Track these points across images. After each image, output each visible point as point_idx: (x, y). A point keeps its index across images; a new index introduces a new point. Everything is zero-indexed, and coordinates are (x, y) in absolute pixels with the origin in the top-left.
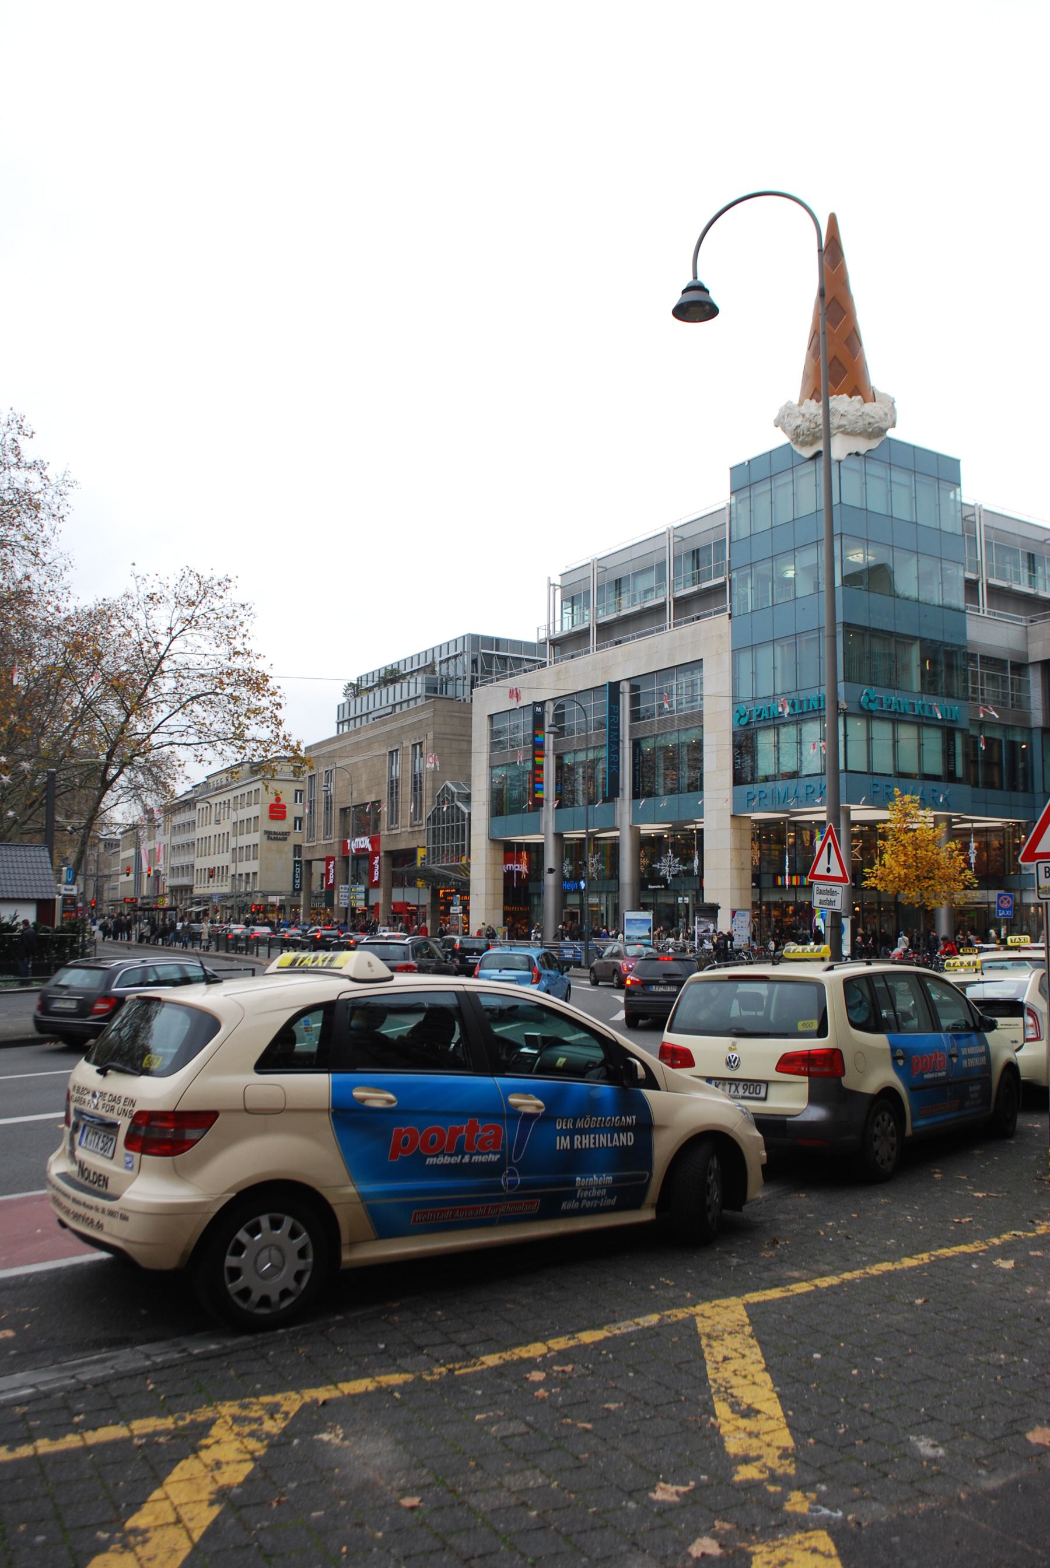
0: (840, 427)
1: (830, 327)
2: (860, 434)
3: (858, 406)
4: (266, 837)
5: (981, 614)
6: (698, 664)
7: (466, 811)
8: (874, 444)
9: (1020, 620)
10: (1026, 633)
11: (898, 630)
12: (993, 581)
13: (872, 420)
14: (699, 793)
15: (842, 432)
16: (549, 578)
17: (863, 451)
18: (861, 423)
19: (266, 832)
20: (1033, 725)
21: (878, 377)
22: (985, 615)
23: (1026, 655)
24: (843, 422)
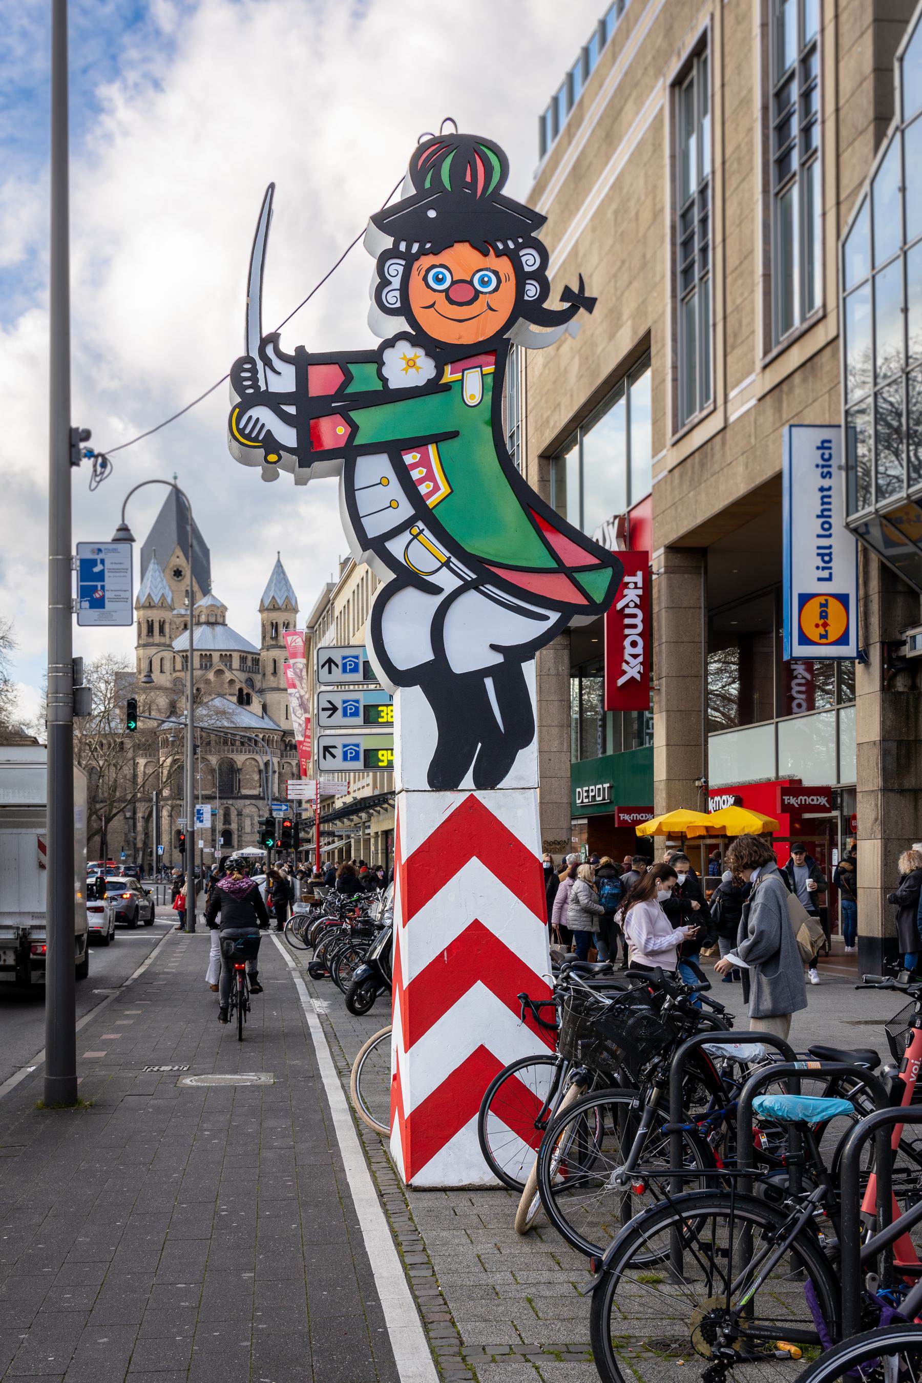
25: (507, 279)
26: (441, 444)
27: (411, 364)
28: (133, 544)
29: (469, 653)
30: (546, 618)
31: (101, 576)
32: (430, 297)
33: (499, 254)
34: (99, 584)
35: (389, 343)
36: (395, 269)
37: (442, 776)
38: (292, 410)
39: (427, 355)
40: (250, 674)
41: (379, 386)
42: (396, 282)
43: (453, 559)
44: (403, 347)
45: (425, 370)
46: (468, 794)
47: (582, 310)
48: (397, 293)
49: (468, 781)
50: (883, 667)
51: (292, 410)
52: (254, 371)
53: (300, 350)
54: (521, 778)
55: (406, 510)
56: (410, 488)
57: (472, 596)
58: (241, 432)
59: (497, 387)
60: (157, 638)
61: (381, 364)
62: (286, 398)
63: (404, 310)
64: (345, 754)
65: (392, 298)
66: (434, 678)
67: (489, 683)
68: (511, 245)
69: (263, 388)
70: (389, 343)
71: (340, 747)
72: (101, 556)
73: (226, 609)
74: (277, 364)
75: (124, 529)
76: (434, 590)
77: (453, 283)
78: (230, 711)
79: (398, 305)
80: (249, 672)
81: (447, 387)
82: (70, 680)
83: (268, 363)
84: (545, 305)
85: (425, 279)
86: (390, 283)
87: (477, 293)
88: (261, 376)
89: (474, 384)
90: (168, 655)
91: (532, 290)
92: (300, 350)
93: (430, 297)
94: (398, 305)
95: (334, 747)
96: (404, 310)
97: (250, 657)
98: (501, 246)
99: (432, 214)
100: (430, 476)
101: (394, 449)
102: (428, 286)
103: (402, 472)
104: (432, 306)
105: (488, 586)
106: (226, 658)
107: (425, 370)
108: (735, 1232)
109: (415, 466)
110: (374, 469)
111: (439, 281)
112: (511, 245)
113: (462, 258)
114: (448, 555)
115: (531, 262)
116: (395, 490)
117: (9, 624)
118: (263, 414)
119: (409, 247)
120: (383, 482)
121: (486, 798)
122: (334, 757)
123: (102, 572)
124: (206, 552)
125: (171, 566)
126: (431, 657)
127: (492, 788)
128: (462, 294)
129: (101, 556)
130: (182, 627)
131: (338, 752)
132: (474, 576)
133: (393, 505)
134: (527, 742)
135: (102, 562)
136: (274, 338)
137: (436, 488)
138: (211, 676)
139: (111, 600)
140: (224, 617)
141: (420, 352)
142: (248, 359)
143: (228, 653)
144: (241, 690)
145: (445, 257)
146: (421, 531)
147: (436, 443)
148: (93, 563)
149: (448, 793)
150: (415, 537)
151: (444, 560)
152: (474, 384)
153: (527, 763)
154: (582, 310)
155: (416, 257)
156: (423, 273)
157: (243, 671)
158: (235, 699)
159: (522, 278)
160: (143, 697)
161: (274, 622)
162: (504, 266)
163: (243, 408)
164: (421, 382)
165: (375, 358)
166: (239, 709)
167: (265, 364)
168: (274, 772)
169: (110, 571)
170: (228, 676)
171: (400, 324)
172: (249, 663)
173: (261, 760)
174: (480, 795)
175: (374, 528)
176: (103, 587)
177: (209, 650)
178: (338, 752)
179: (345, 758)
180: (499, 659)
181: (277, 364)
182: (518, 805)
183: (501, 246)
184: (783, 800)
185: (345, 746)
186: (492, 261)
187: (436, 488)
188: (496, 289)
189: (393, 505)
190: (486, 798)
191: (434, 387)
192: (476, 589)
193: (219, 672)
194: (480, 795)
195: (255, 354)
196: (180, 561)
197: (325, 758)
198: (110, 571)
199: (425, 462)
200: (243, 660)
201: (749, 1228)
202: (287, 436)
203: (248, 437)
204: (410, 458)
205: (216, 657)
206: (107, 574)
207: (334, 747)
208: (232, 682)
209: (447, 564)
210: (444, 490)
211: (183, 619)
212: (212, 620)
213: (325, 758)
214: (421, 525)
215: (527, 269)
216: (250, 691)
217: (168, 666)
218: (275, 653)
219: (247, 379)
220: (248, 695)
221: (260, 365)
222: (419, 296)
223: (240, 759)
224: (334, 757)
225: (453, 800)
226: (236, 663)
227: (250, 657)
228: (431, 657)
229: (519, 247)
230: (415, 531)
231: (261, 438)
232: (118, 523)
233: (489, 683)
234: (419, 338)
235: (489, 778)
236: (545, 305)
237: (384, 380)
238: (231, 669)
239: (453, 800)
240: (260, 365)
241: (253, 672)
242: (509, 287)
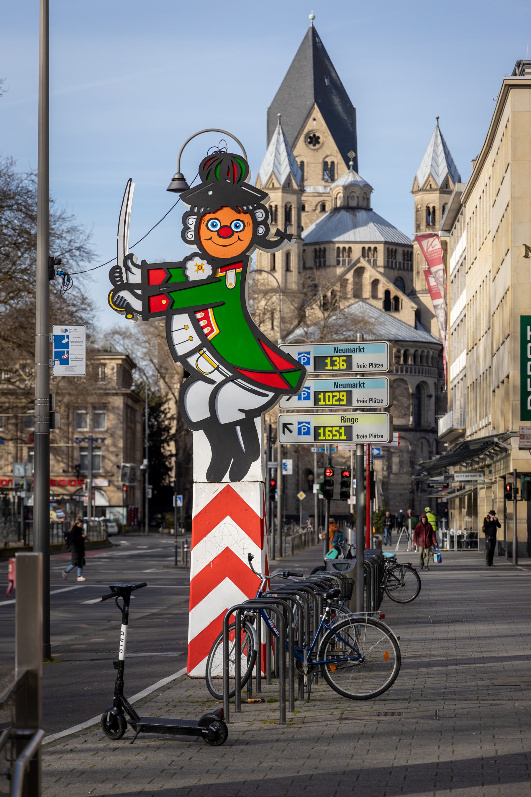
25: (249, 225)
26: (215, 309)
27: (200, 268)
29: (227, 415)
30: (267, 395)
31: (67, 346)
32: (209, 235)
33: (245, 213)
34: (66, 350)
35: (189, 258)
36: (192, 221)
37: (214, 476)
38: (139, 292)
39: (208, 263)
40: (401, 272)
41: (183, 279)
42: (192, 227)
43: (220, 366)
44: (197, 260)
45: (207, 271)
46: (226, 484)
47: (286, 240)
48: (193, 233)
49: (226, 478)
51: (139, 292)
52: (121, 273)
53: (144, 262)
54: (253, 476)
55: (197, 342)
56: (199, 330)
57: (230, 385)
58: (114, 303)
59: (242, 279)
61: (185, 268)
62: (137, 286)
63: (198, 241)
64: (300, 429)
65: (190, 235)
66: (211, 425)
67: (238, 428)
68: (251, 208)
69: (125, 281)
70: (189, 258)
71: (295, 424)
72: (67, 333)
73: (371, 189)
74: (134, 269)
76: (211, 382)
77: (221, 227)
78: (373, 320)
79: (193, 239)
80: (400, 269)
81: (219, 280)
82: (48, 408)
83: (128, 269)
84: (267, 238)
85: (207, 225)
86: (189, 228)
87: (233, 232)
88: (124, 275)
89: (231, 278)
91: (261, 230)
92: (144, 262)
93: (209, 235)
94: (193, 239)
95: (291, 424)
96: (198, 241)
97: (400, 250)
98: (245, 208)
99: (211, 193)
100: (209, 325)
101: (192, 312)
102: (208, 229)
103: (195, 322)
104: (210, 239)
105: (239, 380)
107: (207, 271)
108: (287, 680)
109: (201, 319)
110: (181, 321)
111: (214, 226)
112: (251, 208)
113: (226, 216)
114: (218, 364)
115: (260, 216)
116: (192, 332)
117: (87, 232)
118: (125, 294)
119: (199, 210)
120: (186, 327)
121: (235, 486)
122: (291, 432)
123: (68, 342)
124: (351, 111)
125: (306, 131)
126: (209, 415)
127: (239, 481)
128: (225, 232)
129: (67, 333)
130: (319, 208)
131: (294, 428)
132: (231, 375)
133: (190, 339)
134: (256, 459)
135: (68, 337)
136: (130, 256)
137: (212, 330)
139: (73, 360)
140: (368, 199)
141: (205, 262)
142: (118, 267)
143: (372, 246)
144: (387, 293)
145: (218, 214)
146: (205, 352)
147: (213, 308)
148: (62, 337)
149: (216, 484)
150: (201, 355)
151: (216, 366)
152: (231, 278)
153: (256, 470)
154: (286, 240)
155: (205, 214)
156: (206, 222)
157: (392, 268)
158: (380, 304)
159: (256, 224)
160: (263, 303)
161: (431, 206)
162: (247, 218)
163: (115, 291)
164: (205, 277)
165: (182, 266)
166: (385, 317)
167: (126, 270)
168: (430, 396)
169: (73, 342)
171: (194, 248)
172: (400, 258)
174: (233, 485)
175: (181, 350)
176: (68, 352)
177: (348, 242)
178: (294, 428)
179: (300, 433)
180: (243, 416)
181: (134, 269)
182: (250, 491)
183: (245, 208)
185: (299, 423)
186: (242, 216)
187: (212, 330)
188: (243, 230)
189: (190, 339)
190: (235, 486)
191: (212, 280)
192: (232, 381)
194: (233, 485)
195: (121, 264)
196: (317, 123)
197: (284, 432)
198: (73, 342)
199: (207, 317)
202: (137, 305)
203: (117, 306)
204: (199, 315)
206: (70, 344)
207: (291, 424)
209: (217, 368)
210: (216, 331)
211: (321, 199)
212: (353, 203)
213: (284, 432)
214: (205, 349)
215: (259, 220)
216: (400, 294)
219: (117, 277)
220: (396, 299)
221: (124, 270)
222: (204, 234)
224: (291, 432)
225: (219, 487)
227: (400, 250)
228: (209, 415)
229: (255, 209)
230: (202, 352)
231: (124, 305)
232: (174, 174)
233: (238, 428)
234: (204, 255)
235: (237, 477)
236: (267, 238)
237: (187, 277)
238: (375, 265)
239: (219, 487)
240: (124, 270)
241: (404, 269)
242: (249, 230)
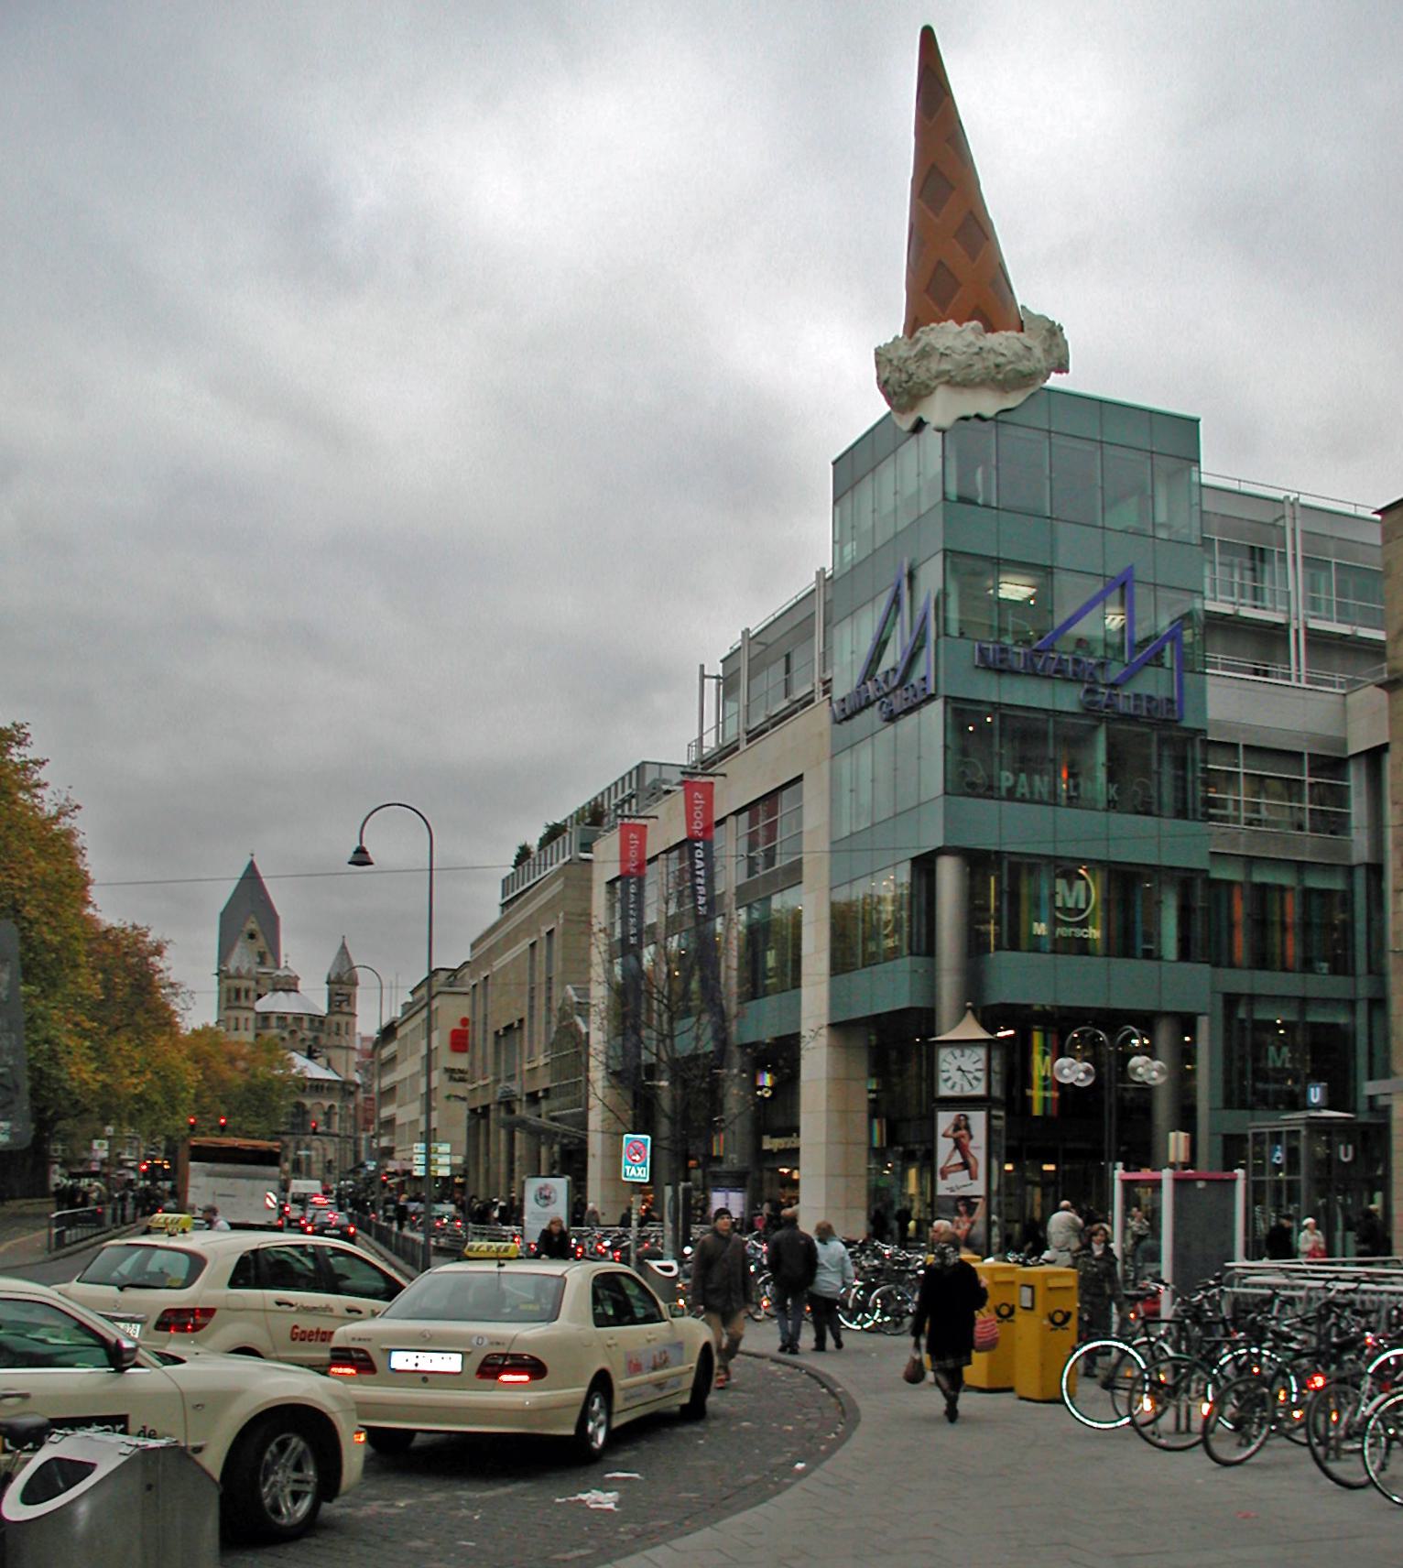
0: (939, 375)
1: (931, 215)
2: (982, 384)
3: (971, 337)
4: (446, 1077)
5: (1293, 683)
6: (799, 778)
7: (584, 1030)
8: (1013, 400)
9: (1332, 684)
10: (1344, 704)
11: (1058, 708)
12: (1313, 624)
13: (1001, 360)
14: (793, 992)
15: (948, 383)
16: (702, 667)
17: (989, 413)
18: (978, 366)
19: (448, 1070)
20: (1355, 860)
21: (1032, 291)
22: (1303, 685)
23: (1343, 743)
24: (946, 366)
28: (1138, 575)
50: (1345, 949)
60: (243, 1003)
67: (61, 1485)
75: (361, 851)
90: (251, 1015)
106: (298, 1018)
138: (286, 1035)
170: (300, 1035)
173: (326, 1104)
184: (1067, 869)
193: (293, 1032)
200: (312, 1021)
201: (1032, 793)
205: (290, 1018)
208: (303, 1040)
217: (251, 1025)
218: (337, 1018)
223: (308, 1102)
226: (306, 1024)
233: (61, 1485)
